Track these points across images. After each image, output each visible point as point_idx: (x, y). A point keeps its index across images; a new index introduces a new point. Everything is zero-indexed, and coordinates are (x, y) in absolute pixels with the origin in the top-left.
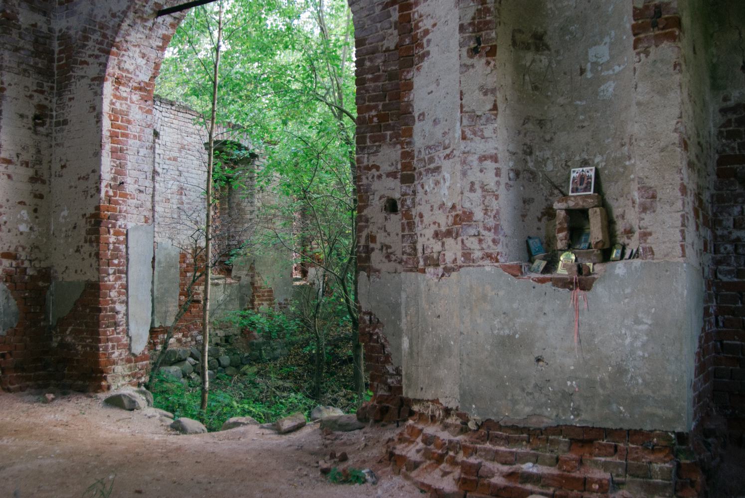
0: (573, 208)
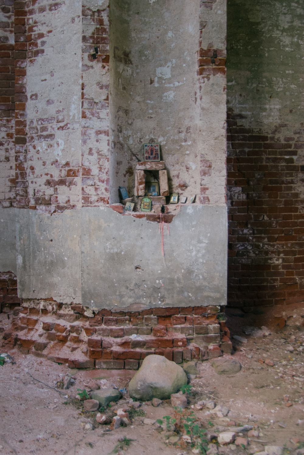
0: (149, 169)
